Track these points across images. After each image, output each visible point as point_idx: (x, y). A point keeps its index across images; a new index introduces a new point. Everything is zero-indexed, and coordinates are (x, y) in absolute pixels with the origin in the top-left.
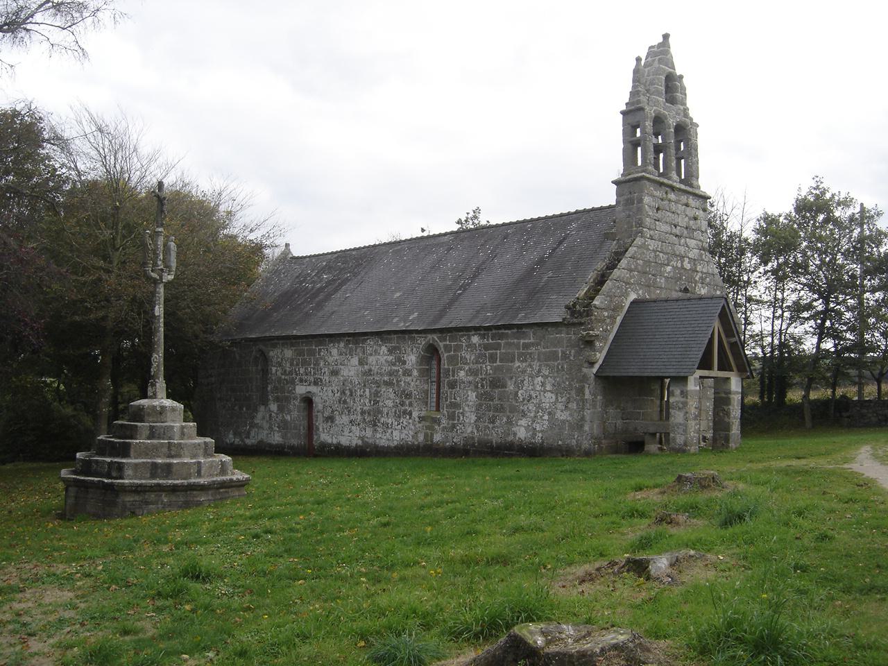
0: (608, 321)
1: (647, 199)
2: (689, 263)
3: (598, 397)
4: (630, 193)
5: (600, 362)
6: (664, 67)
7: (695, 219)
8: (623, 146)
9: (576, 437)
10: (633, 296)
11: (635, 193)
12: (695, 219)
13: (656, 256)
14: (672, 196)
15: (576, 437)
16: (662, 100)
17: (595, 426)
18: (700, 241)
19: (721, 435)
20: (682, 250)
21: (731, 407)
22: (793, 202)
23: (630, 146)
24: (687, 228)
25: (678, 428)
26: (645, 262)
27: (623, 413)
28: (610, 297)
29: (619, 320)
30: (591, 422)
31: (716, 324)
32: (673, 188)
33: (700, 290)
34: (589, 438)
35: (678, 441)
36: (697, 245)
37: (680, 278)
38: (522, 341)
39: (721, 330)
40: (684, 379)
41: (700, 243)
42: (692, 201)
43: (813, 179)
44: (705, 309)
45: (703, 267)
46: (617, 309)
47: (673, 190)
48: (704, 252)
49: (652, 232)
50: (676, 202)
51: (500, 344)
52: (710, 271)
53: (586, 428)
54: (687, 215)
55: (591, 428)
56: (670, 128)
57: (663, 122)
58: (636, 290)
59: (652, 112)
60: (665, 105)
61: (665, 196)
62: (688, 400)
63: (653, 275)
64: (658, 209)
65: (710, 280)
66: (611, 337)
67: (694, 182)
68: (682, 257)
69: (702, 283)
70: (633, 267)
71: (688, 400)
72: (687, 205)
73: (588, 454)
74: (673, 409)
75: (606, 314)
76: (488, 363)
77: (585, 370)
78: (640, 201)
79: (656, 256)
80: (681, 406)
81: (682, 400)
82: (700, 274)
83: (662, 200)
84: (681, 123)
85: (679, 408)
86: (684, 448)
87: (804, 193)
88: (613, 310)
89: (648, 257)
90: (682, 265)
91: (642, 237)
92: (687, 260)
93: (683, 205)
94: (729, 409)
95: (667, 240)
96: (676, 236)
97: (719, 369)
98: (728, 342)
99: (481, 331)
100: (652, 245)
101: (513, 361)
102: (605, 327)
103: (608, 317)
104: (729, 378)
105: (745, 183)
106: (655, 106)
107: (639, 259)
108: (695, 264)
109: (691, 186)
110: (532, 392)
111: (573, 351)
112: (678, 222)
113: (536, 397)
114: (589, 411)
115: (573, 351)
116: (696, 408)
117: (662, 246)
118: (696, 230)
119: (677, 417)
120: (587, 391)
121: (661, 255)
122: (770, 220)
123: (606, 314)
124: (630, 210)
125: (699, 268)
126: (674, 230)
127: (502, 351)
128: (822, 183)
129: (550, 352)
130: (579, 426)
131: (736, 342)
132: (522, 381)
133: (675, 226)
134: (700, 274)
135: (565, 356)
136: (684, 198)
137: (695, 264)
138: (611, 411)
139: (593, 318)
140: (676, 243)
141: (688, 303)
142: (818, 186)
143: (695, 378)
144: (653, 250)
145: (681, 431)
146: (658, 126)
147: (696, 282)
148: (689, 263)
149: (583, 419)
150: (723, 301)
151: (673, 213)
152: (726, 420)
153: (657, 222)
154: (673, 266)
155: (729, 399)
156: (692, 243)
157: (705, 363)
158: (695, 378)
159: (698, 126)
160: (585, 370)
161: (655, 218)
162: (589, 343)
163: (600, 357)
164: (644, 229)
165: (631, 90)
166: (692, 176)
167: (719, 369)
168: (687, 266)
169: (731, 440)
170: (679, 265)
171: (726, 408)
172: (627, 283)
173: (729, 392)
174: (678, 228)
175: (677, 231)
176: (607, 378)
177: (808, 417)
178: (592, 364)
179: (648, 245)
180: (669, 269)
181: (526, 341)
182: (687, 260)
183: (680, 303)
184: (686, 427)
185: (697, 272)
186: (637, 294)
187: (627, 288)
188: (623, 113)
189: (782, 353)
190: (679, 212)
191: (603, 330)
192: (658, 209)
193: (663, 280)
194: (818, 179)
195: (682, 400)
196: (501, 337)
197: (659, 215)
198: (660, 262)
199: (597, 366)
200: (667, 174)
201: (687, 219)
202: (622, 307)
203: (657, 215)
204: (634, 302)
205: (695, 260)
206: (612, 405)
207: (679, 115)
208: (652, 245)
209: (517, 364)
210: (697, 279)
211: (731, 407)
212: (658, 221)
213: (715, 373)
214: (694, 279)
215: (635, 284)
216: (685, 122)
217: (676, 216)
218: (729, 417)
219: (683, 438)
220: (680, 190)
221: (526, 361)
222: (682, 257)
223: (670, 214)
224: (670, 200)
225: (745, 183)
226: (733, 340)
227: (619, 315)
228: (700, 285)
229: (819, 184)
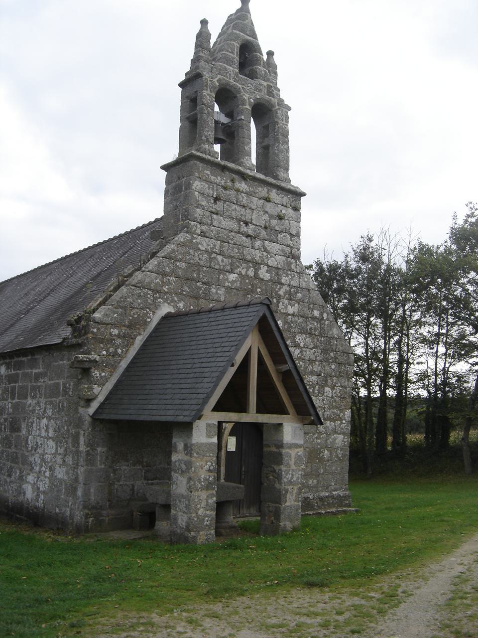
0: (118, 341)
1: (197, 185)
2: (267, 271)
3: (99, 449)
4: (179, 178)
5: (101, 398)
6: (238, 32)
7: (280, 218)
8: (180, 125)
9: (70, 504)
10: (166, 309)
11: (183, 178)
12: (280, 218)
13: (211, 259)
14: (243, 186)
15: (70, 504)
16: (233, 69)
17: (92, 490)
18: (288, 246)
19: (271, 509)
20: (257, 255)
21: (283, 468)
22: (449, 231)
23: (187, 123)
24: (265, 228)
25: (180, 501)
26: (190, 265)
27: (147, 471)
28: (125, 308)
29: (139, 341)
30: (84, 484)
31: (252, 342)
32: (244, 177)
33: (286, 307)
34: (81, 507)
35: (180, 521)
36: (283, 251)
37: (253, 291)
38: (34, 371)
39: (264, 352)
40: (187, 427)
41: (288, 250)
42: (274, 194)
43: (467, 205)
44: (237, 320)
45: (292, 279)
46: (136, 325)
47: (245, 179)
48: (293, 261)
49: (204, 228)
50: (248, 194)
51: (17, 375)
52: (304, 285)
53: (80, 493)
54: (266, 212)
55: (86, 493)
56: (243, 104)
57: (235, 97)
58: (173, 300)
59: (215, 80)
60: (237, 76)
61: (229, 184)
62: (193, 459)
63: (204, 283)
64: (217, 199)
65: (304, 296)
66: (124, 364)
67: (281, 174)
68: (257, 265)
69: (290, 299)
70: (167, 269)
71: (193, 459)
72: (268, 200)
73: (80, 530)
74: (175, 472)
75: (115, 332)
76: (9, 400)
77: (81, 410)
78: (188, 186)
79: (211, 259)
80: (184, 467)
81: (186, 458)
82: (286, 288)
83: (225, 188)
84: (262, 101)
85: (183, 472)
86: (187, 533)
87: (460, 222)
88: (129, 327)
89: (197, 259)
90: (256, 273)
91: (187, 232)
92: (264, 269)
93: (260, 199)
94: (280, 470)
95: (232, 239)
96: (248, 236)
97: (259, 411)
98: (278, 372)
99: (6, 359)
100: (205, 244)
101: (26, 398)
102: (111, 350)
103: (119, 336)
104: (280, 425)
105: (363, 190)
106: (219, 74)
107: (180, 260)
108: (277, 274)
109: (276, 177)
110: (38, 438)
111: (72, 384)
112: (252, 219)
113: (41, 444)
114: (82, 469)
115: (72, 384)
116: (210, 471)
117: (221, 246)
118: (281, 232)
119: (180, 485)
120: (82, 440)
121: (220, 258)
122: (424, 251)
123: (115, 332)
124: (176, 200)
125: (284, 280)
126: (244, 228)
127: (20, 384)
128: (476, 209)
129: (54, 383)
130: (72, 490)
131: (289, 371)
132: (32, 423)
133: (246, 224)
134: (286, 288)
135: (65, 392)
136: (263, 191)
137: (277, 274)
138: (124, 468)
139: (90, 336)
140: (246, 244)
141: (221, 314)
142: (473, 214)
143: (208, 425)
144: (206, 251)
145: (182, 506)
146: (231, 105)
147: (279, 297)
148: (267, 271)
149: (76, 480)
150: (263, 310)
151: (244, 206)
152: (277, 485)
153: (215, 216)
154: (240, 274)
155: (280, 454)
156: (274, 247)
157: (233, 399)
158: (208, 425)
159: (290, 109)
160: (81, 410)
161: (210, 209)
162: (84, 371)
163: (101, 393)
164: (192, 223)
165: (192, 58)
166: (278, 166)
167: (259, 411)
168: (264, 273)
169: (282, 516)
170: (251, 273)
171: (276, 468)
172: (155, 291)
173: (280, 445)
174: (251, 227)
175: (250, 230)
176: (102, 421)
177: (467, 461)
178: (89, 401)
179: (198, 244)
180: (232, 277)
181: (37, 371)
182: (264, 269)
183: (212, 315)
184: (189, 500)
185: (282, 284)
186: (175, 306)
187: (156, 298)
188: (182, 85)
189: (444, 393)
190: (254, 207)
191: (108, 355)
192: (217, 199)
193: (222, 291)
194: (472, 206)
195: (186, 458)
196: (19, 366)
197: (219, 206)
198: (217, 267)
199: (95, 405)
200: (239, 159)
201: (266, 217)
202: (146, 324)
203: (215, 207)
204: (167, 317)
205: (278, 268)
206: (127, 461)
207: (260, 91)
208: (205, 244)
209: (29, 401)
210: (281, 293)
211: (283, 468)
212: (217, 214)
213: (252, 416)
214: (276, 293)
215: (171, 293)
216: (269, 101)
217: (248, 211)
218: (280, 484)
219: (185, 518)
220: (254, 179)
221: (36, 398)
222: (257, 265)
223: (238, 208)
224: (238, 190)
225: (363, 190)
226: (284, 368)
227: (140, 334)
228: (286, 302)
229: (473, 211)
